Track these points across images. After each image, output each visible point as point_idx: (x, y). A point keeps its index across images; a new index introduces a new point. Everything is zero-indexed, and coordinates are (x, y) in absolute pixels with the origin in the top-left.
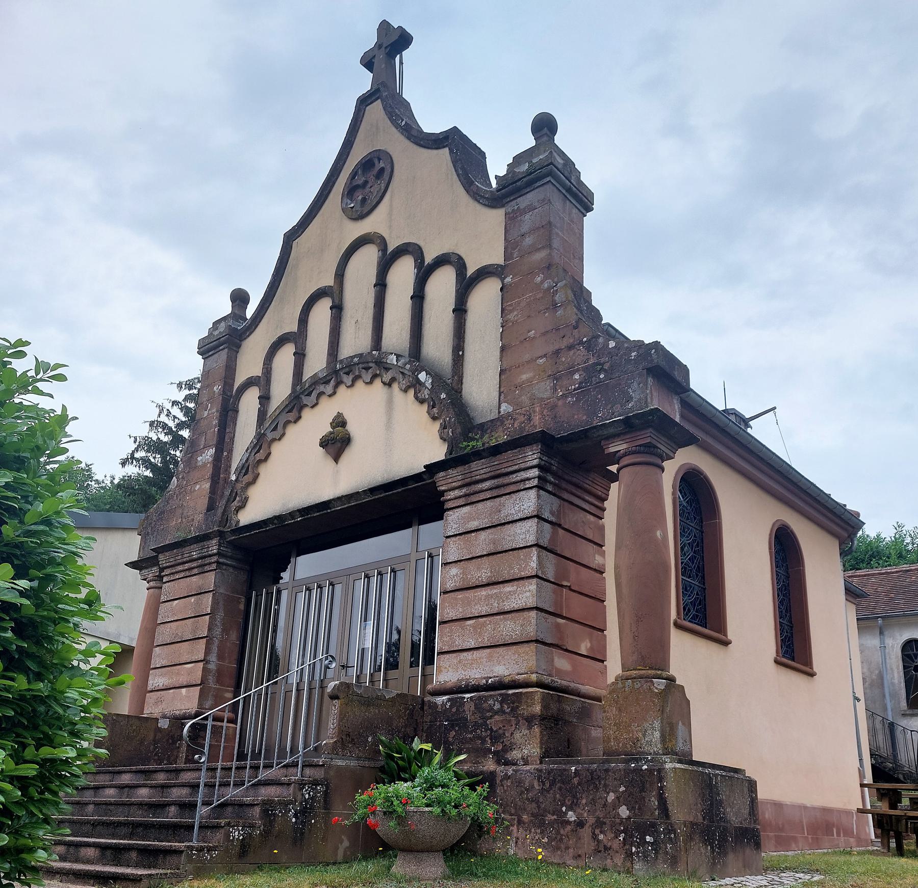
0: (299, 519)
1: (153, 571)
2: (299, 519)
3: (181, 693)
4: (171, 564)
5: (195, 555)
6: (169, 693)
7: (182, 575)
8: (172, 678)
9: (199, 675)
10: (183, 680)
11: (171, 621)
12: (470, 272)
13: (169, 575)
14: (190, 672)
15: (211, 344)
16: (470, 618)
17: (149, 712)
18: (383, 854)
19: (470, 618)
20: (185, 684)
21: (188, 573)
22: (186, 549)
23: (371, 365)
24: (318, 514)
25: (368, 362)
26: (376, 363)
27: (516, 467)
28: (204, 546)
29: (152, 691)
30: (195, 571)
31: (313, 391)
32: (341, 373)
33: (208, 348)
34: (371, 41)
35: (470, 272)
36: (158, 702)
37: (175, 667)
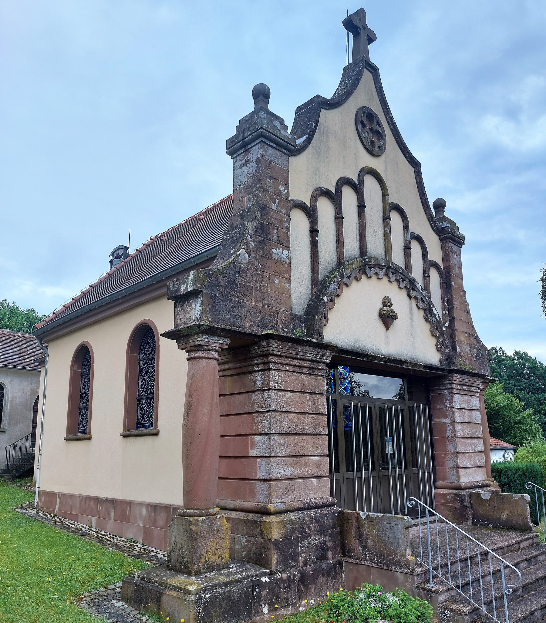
0: (382, 363)
1: (222, 342)
2: (382, 363)
3: (312, 483)
4: (283, 354)
5: (309, 356)
6: (298, 482)
7: (292, 369)
8: (300, 469)
9: (327, 468)
10: (312, 471)
11: (290, 412)
12: (333, 191)
13: (278, 363)
14: (318, 464)
15: (279, 140)
16: (467, 452)
17: (279, 501)
18: (208, 618)
19: (467, 452)
20: (315, 474)
21: (298, 370)
22: (302, 348)
23: (407, 280)
24: (393, 365)
25: (406, 277)
26: (410, 281)
27: (475, 385)
28: (320, 353)
29: (278, 480)
30: (306, 370)
31: (373, 268)
32: (390, 271)
33: (274, 139)
34: (371, 23)
35: (333, 191)
36: (286, 492)
37: (301, 458)
